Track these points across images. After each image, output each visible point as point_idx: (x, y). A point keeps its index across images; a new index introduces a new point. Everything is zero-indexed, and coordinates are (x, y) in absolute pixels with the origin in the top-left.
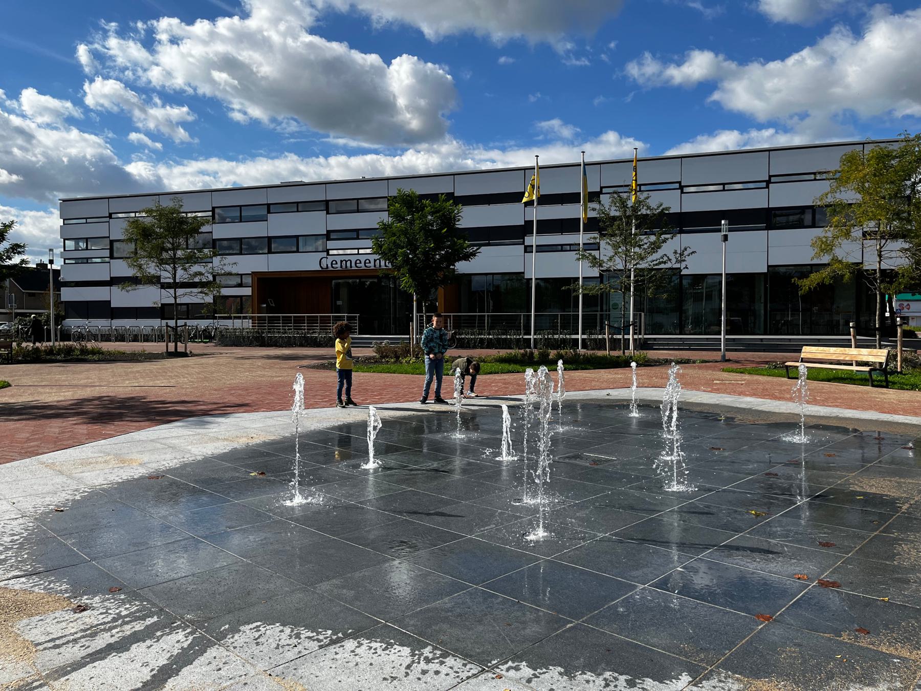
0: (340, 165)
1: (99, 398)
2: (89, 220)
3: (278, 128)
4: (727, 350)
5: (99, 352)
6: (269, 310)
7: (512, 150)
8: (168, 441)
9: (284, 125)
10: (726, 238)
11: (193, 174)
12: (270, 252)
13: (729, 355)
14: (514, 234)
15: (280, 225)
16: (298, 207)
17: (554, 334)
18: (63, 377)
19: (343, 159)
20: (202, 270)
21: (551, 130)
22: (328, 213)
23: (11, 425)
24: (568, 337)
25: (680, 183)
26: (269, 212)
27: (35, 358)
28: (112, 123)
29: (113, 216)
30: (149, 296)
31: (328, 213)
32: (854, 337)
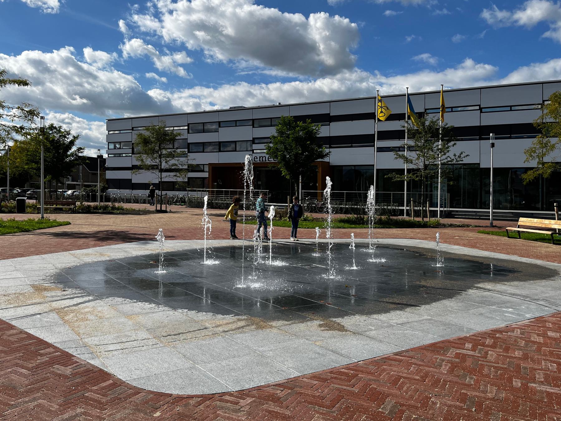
0: (276, 89)
1: (107, 231)
2: (121, 132)
3: (234, 66)
4: (494, 220)
5: (122, 209)
6: (219, 186)
7: (391, 76)
8: (125, 249)
9: (237, 64)
10: (493, 145)
11: (186, 98)
12: (220, 151)
13: (495, 223)
14: (365, 140)
15: (226, 135)
16: (236, 123)
17: (388, 206)
18: (97, 221)
19: (278, 84)
20: (176, 162)
21: (422, 61)
22: (253, 127)
23: (64, 240)
24: (397, 208)
25: (480, 106)
26: (220, 127)
27: (87, 211)
28: (138, 66)
29: (134, 129)
30: (152, 177)
31: (253, 127)
32: (557, 213)
